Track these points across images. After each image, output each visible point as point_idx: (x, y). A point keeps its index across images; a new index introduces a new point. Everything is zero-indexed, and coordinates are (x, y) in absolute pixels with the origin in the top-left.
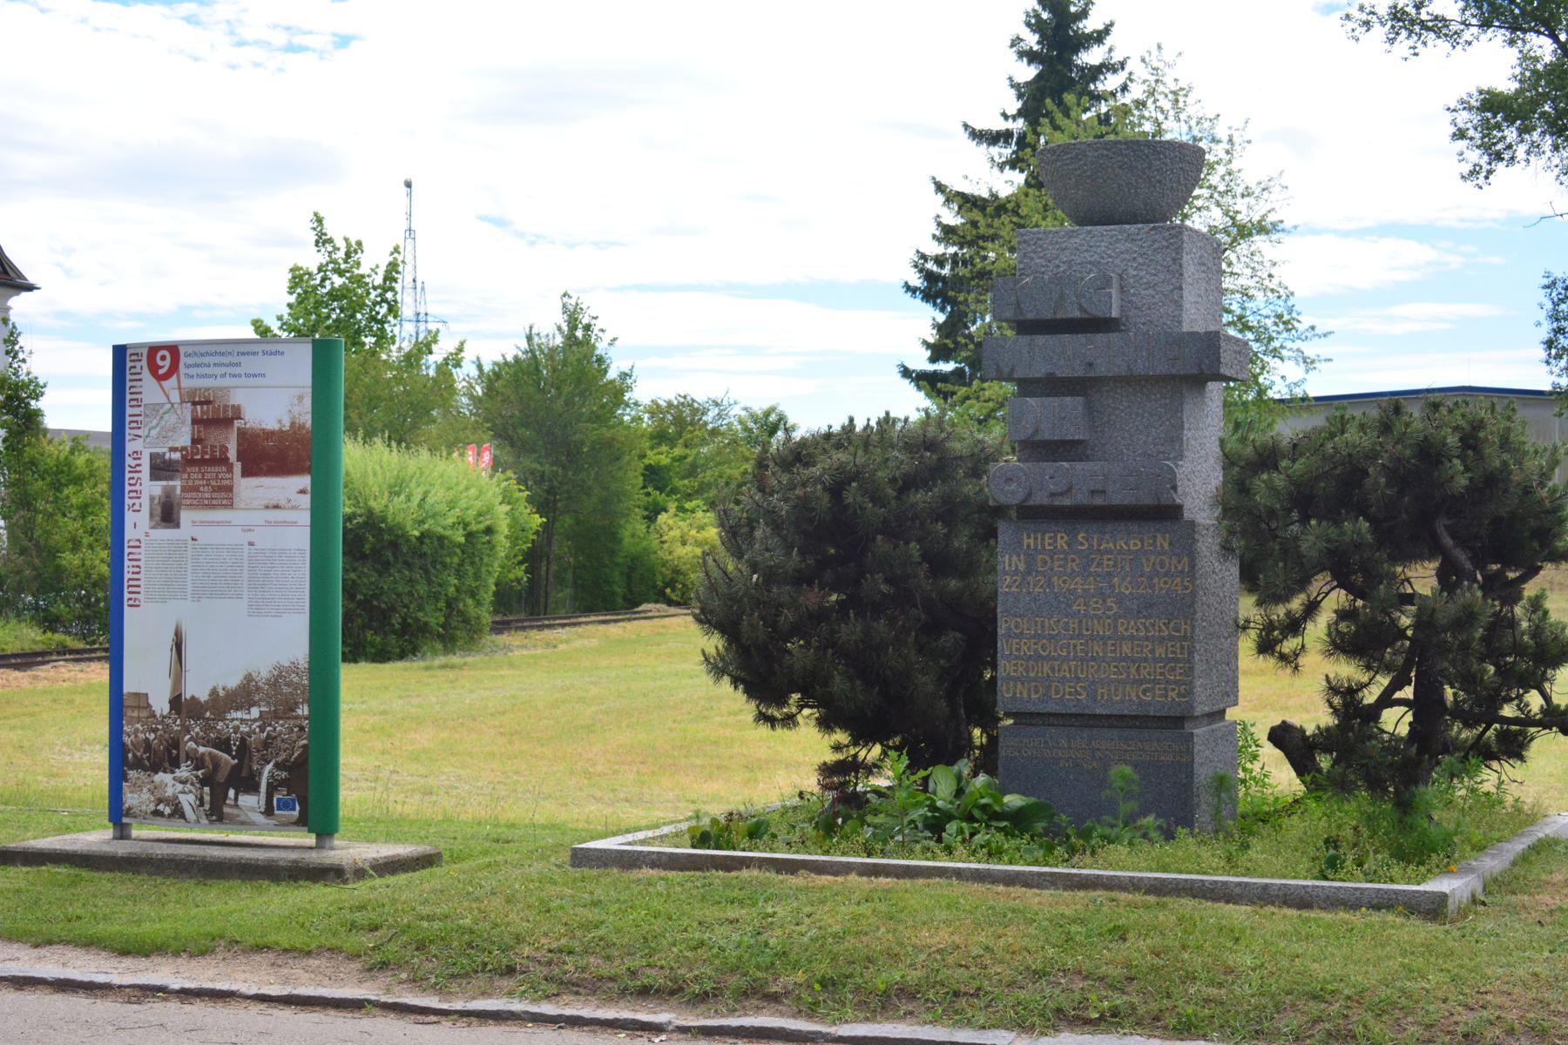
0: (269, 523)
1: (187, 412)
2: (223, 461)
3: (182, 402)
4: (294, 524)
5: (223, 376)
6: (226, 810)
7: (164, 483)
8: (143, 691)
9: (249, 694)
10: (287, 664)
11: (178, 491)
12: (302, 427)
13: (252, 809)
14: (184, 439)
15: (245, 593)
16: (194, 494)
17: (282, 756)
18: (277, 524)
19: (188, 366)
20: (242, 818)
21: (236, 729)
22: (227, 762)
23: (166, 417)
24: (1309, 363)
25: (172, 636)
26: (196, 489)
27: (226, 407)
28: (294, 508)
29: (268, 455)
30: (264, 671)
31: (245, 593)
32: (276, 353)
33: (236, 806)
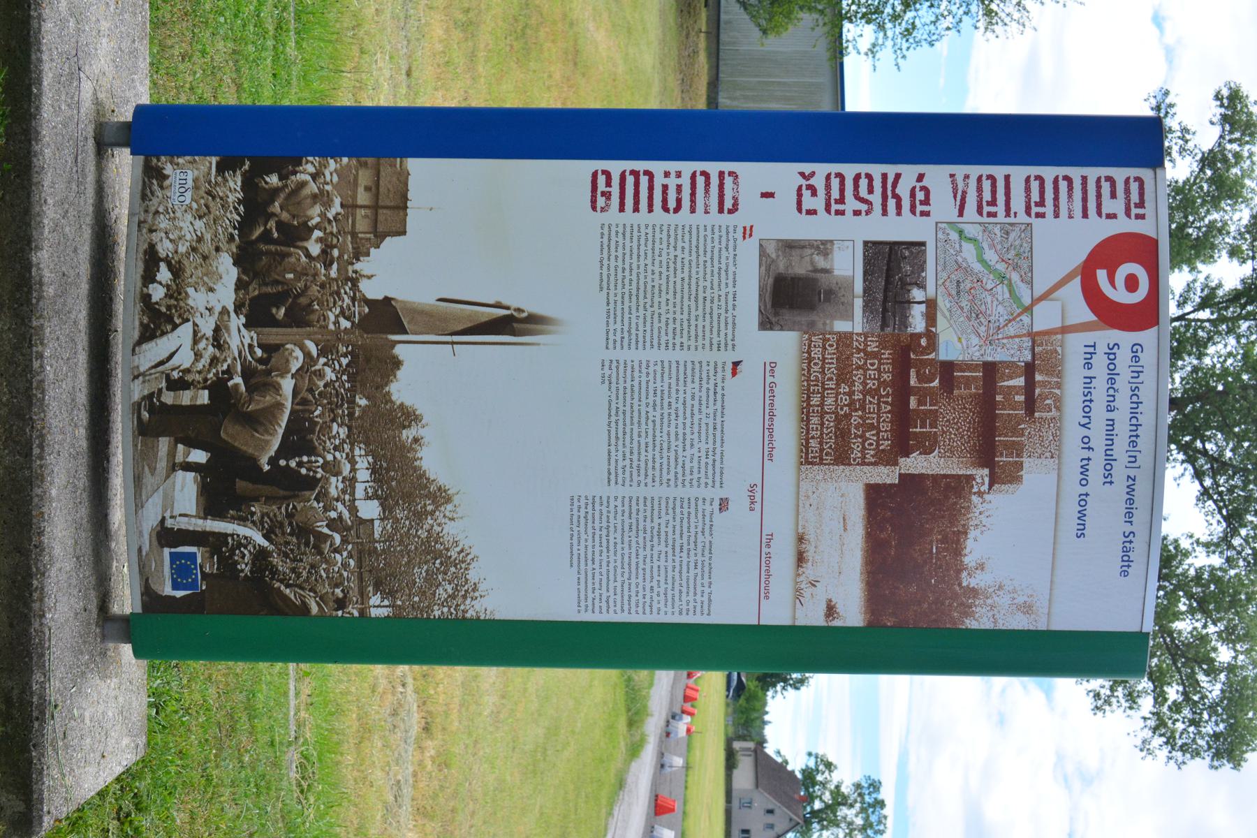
0: (766, 541)
1: (1013, 352)
2: (903, 445)
3: (1033, 336)
4: (764, 593)
5: (1086, 444)
6: (164, 443)
7: (859, 287)
8: (413, 218)
9: (408, 497)
10: (473, 576)
11: (841, 326)
12: (967, 611)
13: (168, 502)
14: (956, 343)
15: (621, 491)
16: (832, 369)
17: (282, 566)
18: (765, 560)
19: (1111, 354)
20: (149, 480)
21: (332, 468)
22: (264, 445)
23: (1002, 291)
24: (872, 51)
25: (531, 307)
26: (843, 376)
27: (1018, 449)
28: (798, 594)
29: (911, 529)
30: (458, 528)
31: (621, 491)
32: (1127, 562)
33: (173, 467)
